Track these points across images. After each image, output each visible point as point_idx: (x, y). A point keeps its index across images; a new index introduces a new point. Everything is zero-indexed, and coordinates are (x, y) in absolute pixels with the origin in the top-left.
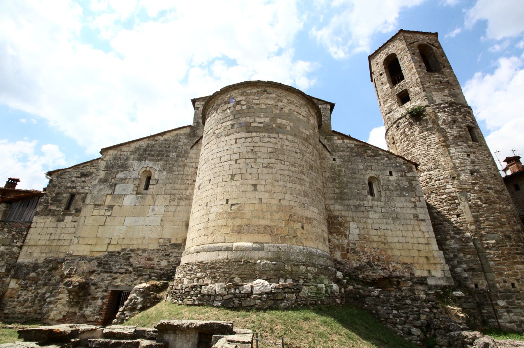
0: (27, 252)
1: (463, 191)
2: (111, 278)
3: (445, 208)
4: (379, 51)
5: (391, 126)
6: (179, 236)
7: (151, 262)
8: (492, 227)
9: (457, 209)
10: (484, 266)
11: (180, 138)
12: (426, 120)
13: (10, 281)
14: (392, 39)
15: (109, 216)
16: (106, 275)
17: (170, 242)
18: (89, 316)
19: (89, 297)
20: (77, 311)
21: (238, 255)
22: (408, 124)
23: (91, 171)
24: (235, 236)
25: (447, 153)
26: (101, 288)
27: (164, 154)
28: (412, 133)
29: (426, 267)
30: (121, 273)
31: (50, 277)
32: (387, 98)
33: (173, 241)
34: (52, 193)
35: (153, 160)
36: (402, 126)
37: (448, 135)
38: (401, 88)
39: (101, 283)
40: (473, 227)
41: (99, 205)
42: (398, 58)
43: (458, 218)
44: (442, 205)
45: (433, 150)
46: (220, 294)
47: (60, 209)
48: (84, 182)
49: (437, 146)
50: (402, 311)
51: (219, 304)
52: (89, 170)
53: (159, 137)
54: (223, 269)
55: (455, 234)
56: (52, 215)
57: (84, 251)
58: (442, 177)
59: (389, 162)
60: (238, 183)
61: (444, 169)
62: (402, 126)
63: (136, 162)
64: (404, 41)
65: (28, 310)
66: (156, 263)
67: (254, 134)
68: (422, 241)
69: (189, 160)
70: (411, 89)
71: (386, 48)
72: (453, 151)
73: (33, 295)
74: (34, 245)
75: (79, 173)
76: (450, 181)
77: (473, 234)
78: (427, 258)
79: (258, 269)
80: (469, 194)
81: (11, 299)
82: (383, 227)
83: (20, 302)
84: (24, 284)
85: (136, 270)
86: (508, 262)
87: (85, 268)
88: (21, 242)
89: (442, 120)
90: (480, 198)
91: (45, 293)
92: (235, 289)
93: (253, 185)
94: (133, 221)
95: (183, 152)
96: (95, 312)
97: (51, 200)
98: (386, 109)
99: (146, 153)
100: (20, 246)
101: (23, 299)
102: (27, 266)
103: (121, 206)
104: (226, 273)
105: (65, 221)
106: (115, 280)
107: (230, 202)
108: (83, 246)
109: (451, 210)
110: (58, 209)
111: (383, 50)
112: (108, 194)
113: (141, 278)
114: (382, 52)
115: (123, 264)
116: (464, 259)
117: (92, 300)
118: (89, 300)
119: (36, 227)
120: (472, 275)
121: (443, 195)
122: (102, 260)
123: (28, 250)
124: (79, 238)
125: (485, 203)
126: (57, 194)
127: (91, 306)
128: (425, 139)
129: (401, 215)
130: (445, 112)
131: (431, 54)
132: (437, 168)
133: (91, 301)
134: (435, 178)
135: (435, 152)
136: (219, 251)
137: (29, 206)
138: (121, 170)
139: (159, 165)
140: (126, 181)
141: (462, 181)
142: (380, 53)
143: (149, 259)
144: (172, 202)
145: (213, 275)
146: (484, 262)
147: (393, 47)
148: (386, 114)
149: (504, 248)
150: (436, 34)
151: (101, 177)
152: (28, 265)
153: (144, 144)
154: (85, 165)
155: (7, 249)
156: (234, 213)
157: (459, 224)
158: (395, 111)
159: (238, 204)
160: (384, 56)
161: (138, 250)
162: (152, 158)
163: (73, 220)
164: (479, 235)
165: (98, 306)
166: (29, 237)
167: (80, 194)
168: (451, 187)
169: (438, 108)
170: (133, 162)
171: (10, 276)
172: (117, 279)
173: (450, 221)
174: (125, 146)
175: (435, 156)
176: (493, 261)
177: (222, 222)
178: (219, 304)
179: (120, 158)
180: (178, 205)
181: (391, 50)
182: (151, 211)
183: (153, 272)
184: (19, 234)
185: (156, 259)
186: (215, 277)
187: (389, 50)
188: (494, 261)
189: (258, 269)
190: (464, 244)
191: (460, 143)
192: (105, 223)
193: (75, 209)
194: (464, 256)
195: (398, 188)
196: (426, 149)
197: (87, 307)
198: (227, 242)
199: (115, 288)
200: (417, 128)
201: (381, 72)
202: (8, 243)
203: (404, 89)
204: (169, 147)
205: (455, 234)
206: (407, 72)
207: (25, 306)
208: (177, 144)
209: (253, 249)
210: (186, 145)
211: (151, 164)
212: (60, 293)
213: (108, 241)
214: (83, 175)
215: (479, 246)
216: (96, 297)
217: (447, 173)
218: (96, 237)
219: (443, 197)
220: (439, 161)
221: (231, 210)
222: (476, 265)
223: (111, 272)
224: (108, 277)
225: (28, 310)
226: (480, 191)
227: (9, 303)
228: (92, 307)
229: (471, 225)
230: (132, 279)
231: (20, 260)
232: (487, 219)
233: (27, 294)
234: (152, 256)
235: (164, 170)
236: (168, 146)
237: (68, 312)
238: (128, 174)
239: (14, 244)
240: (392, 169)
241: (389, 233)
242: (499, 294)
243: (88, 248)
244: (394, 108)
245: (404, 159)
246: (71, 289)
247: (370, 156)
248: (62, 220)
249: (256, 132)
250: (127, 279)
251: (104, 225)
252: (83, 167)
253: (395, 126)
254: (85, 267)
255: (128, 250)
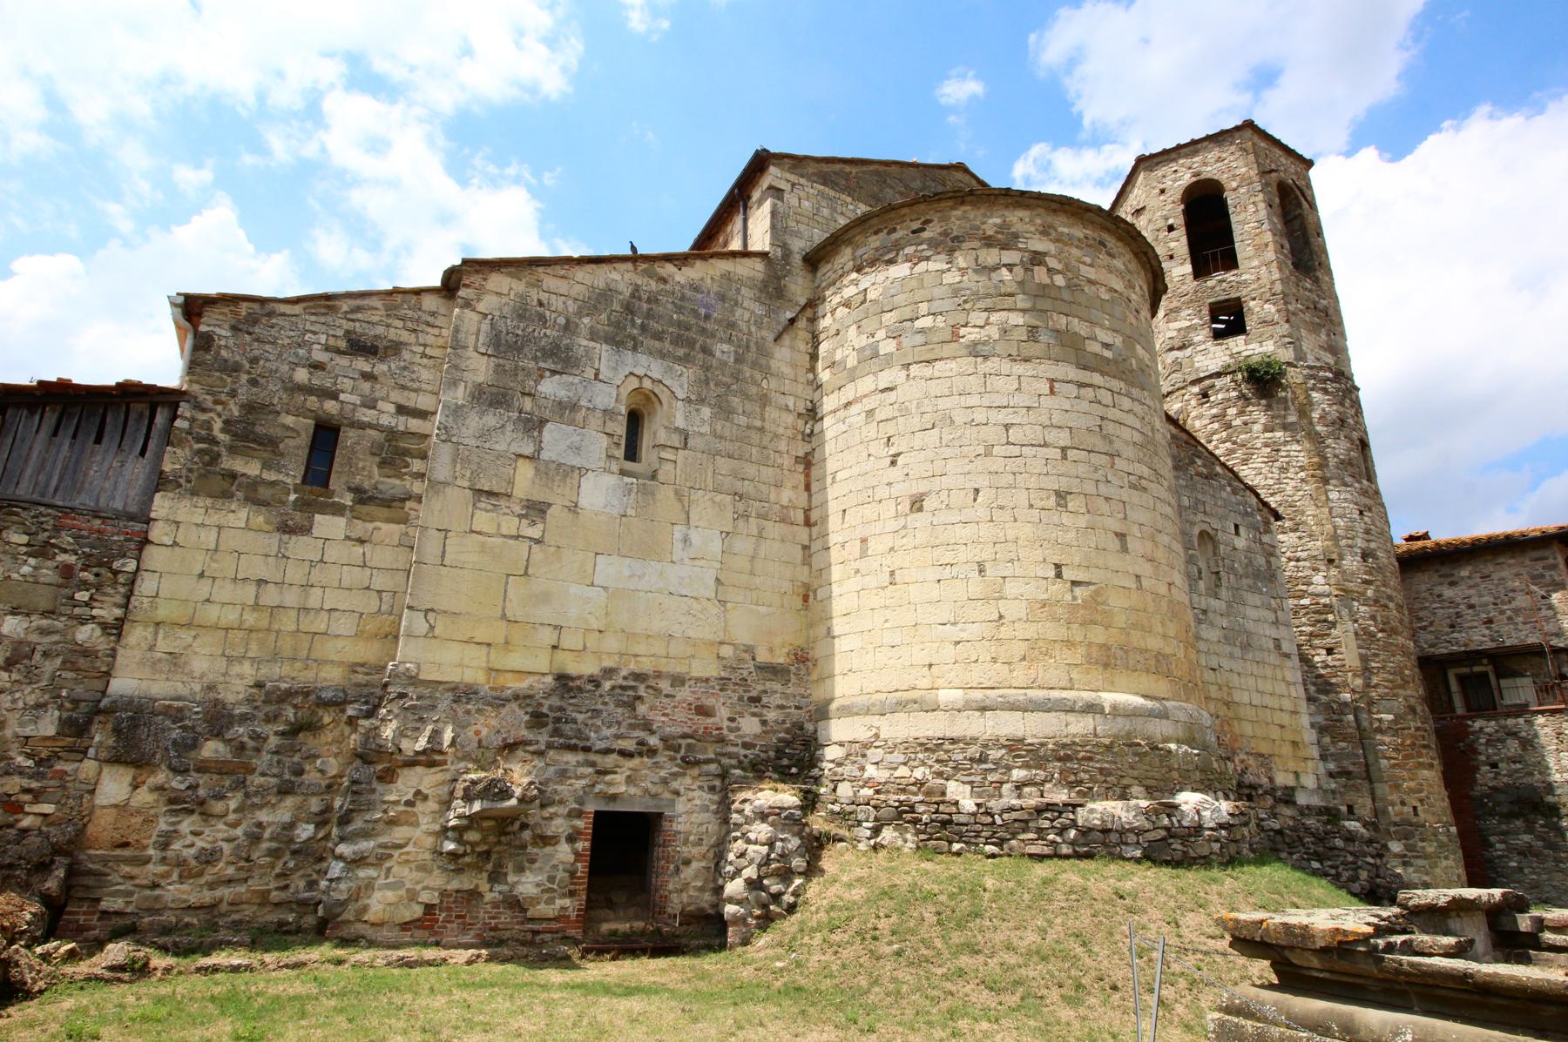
0: (151, 648)
1: (1346, 595)
2: (590, 770)
3: (1303, 629)
4: (1173, 155)
5: (1183, 388)
6: (778, 641)
7: (710, 721)
8: (1390, 685)
9: (1328, 635)
10: (1371, 768)
11: (738, 291)
12: (1285, 400)
13: (100, 773)
14: (1219, 138)
15: (538, 541)
16: (571, 758)
17: (754, 659)
18: (534, 900)
19: (527, 835)
20: (484, 887)
21: (1120, 726)
22: (1238, 398)
23: (392, 334)
24: (1097, 675)
25: (1324, 498)
26: (561, 802)
27: (695, 342)
28: (1246, 424)
29: (1292, 765)
30: (625, 754)
31: (296, 759)
32: (1179, 304)
33: (763, 657)
34: (223, 397)
35: (663, 355)
36: (1220, 396)
37: (1329, 453)
38: (1224, 290)
39: (559, 788)
40: (1359, 682)
41: (490, 494)
42: (1229, 202)
43: (1330, 658)
44: (1297, 622)
45: (1293, 483)
46: (1136, 828)
47: (281, 477)
48: (367, 376)
49: (1302, 474)
50: (1330, 863)
51: (1138, 853)
52: (380, 330)
53: (669, 268)
54: (1097, 762)
55: (1319, 691)
56: (247, 499)
57: (461, 665)
58: (1304, 555)
59: (1233, 499)
60: (1082, 521)
61: (1310, 536)
62: (1220, 396)
63: (604, 350)
64: (1251, 157)
65: (225, 892)
66: (726, 724)
67: (1097, 378)
68: (1287, 704)
69: (774, 384)
70: (1252, 304)
71: (1195, 153)
72: (1333, 495)
73: (239, 832)
74: (184, 620)
75: (340, 333)
76: (1323, 568)
77: (1357, 696)
78: (1294, 743)
79: (1176, 766)
80: (1356, 604)
81: (126, 853)
82: (1226, 664)
83: (181, 863)
84: (183, 787)
85: (669, 743)
86: (1411, 763)
87: (485, 732)
88: (119, 606)
89: (1319, 411)
90: (1373, 618)
91: (291, 826)
92: (1169, 816)
93: (1117, 534)
94: (626, 573)
95: (753, 348)
96: (555, 887)
97: (223, 431)
98: (1174, 334)
99: (633, 321)
100: (110, 620)
101: (192, 851)
102: (177, 715)
103: (574, 508)
104: (1110, 774)
105: (316, 532)
106: (608, 778)
107: (1067, 574)
108: (457, 647)
109: (1317, 636)
110: (270, 476)
111: (1186, 156)
112: (520, 456)
113: (695, 772)
114: (1181, 161)
115: (625, 724)
116: (1333, 750)
117: (535, 844)
118: (524, 847)
119: (175, 544)
120: (1345, 786)
121: (1301, 597)
122: (540, 705)
123: (160, 642)
124: (431, 615)
125: (1382, 631)
126: (250, 408)
127: (537, 865)
128: (1278, 450)
129: (1255, 638)
130: (1325, 391)
131: (1296, 218)
132: (1296, 530)
133: (530, 849)
134: (1288, 554)
135: (1297, 489)
136: (1067, 711)
137: (105, 440)
138: (553, 367)
139: (684, 379)
140: (579, 416)
141: (1345, 572)
142: (1174, 160)
143: (703, 711)
144: (741, 523)
145: (1072, 778)
146: (1371, 759)
147: (1217, 161)
148: (1171, 349)
149: (1406, 732)
150: (1309, 164)
151: (480, 379)
152: (180, 710)
153: (621, 279)
154: (359, 302)
155: (43, 632)
156: (1084, 607)
157: (1329, 670)
158: (1199, 348)
159: (1089, 584)
160: (1186, 179)
161: (659, 675)
162: (657, 344)
163: (353, 535)
164: (1365, 700)
165: (561, 867)
166: (146, 585)
167: (363, 426)
168: (1323, 581)
169: (1313, 377)
170: (592, 344)
171: (91, 752)
172: (615, 773)
173: (1311, 661)
174: (549, 270)
175: (1296, 498)
176: (1386, 758)
177: (1052, 631)
178: (1138, 853)
179: (542, 319)
180: (760, 536)
181: (1211, 165)
182: (680, 545)
183: (724, 755)
184: (100, 565)
185: (723, 713)
186: (1080, 782)
187: (1205, 164)
188: (1389, 758)
189: (1176, 766)
190: (1335, 717)
191: (1348, 479)
192: (527, 568)
193: (350, 489)
194: (1333, 742)
195: (1250, 569)
196: (1277, 476)
197: (520, 870)
198: (1078, 689)
199: (607, 804)
200: (1258, 416)
201: (1171, 221)
202: (44, 604)
203: (1233, 295)
204: (707, 317)
205: (1319, 691)
206: (1250, 251)
207: (207, 878)
208: (732, 312)
209: (1151, 714)
210: (760, 327)
211: (656, 369)
212: (392, 822)
213: (548, 637)
214: (359, 347)
215: (1365, 724)
216: (549, 833)
217: (1317, 546)
218: (504, 616)
219: (1303, 602)
220: (1303, 513)
221: (1074, 598)
222: (1354, 764)
223: (587, 750)
224: (579, 764)
225: (225, 892)
226: (1376, 601)
227: (126, 869)
228: (540, 869)
229: (1355, 675)
230: (663, 773)
231: (123, 684)
232: (1383, 668)
233: (207, 831)
234: (709, 702)
235: (702, 401)
236: (703, 311)
237: (444, 894)
238: (581, 390)
239: (77, 611)
240: (1239, 520)
241: (1235, 680)
242: (1392, 829)
243: (477, 657)
244: (1196, 339)
245: (1257, 495)
246: (512, 808)
247: (1199, 474)
248: (305, 530)
249: (1103, 373)
250: (646, 775)
251: (526, 574)
252: (353, 311)
253: (1196, 389)
254: (487, 726)
255: (624, 673)
